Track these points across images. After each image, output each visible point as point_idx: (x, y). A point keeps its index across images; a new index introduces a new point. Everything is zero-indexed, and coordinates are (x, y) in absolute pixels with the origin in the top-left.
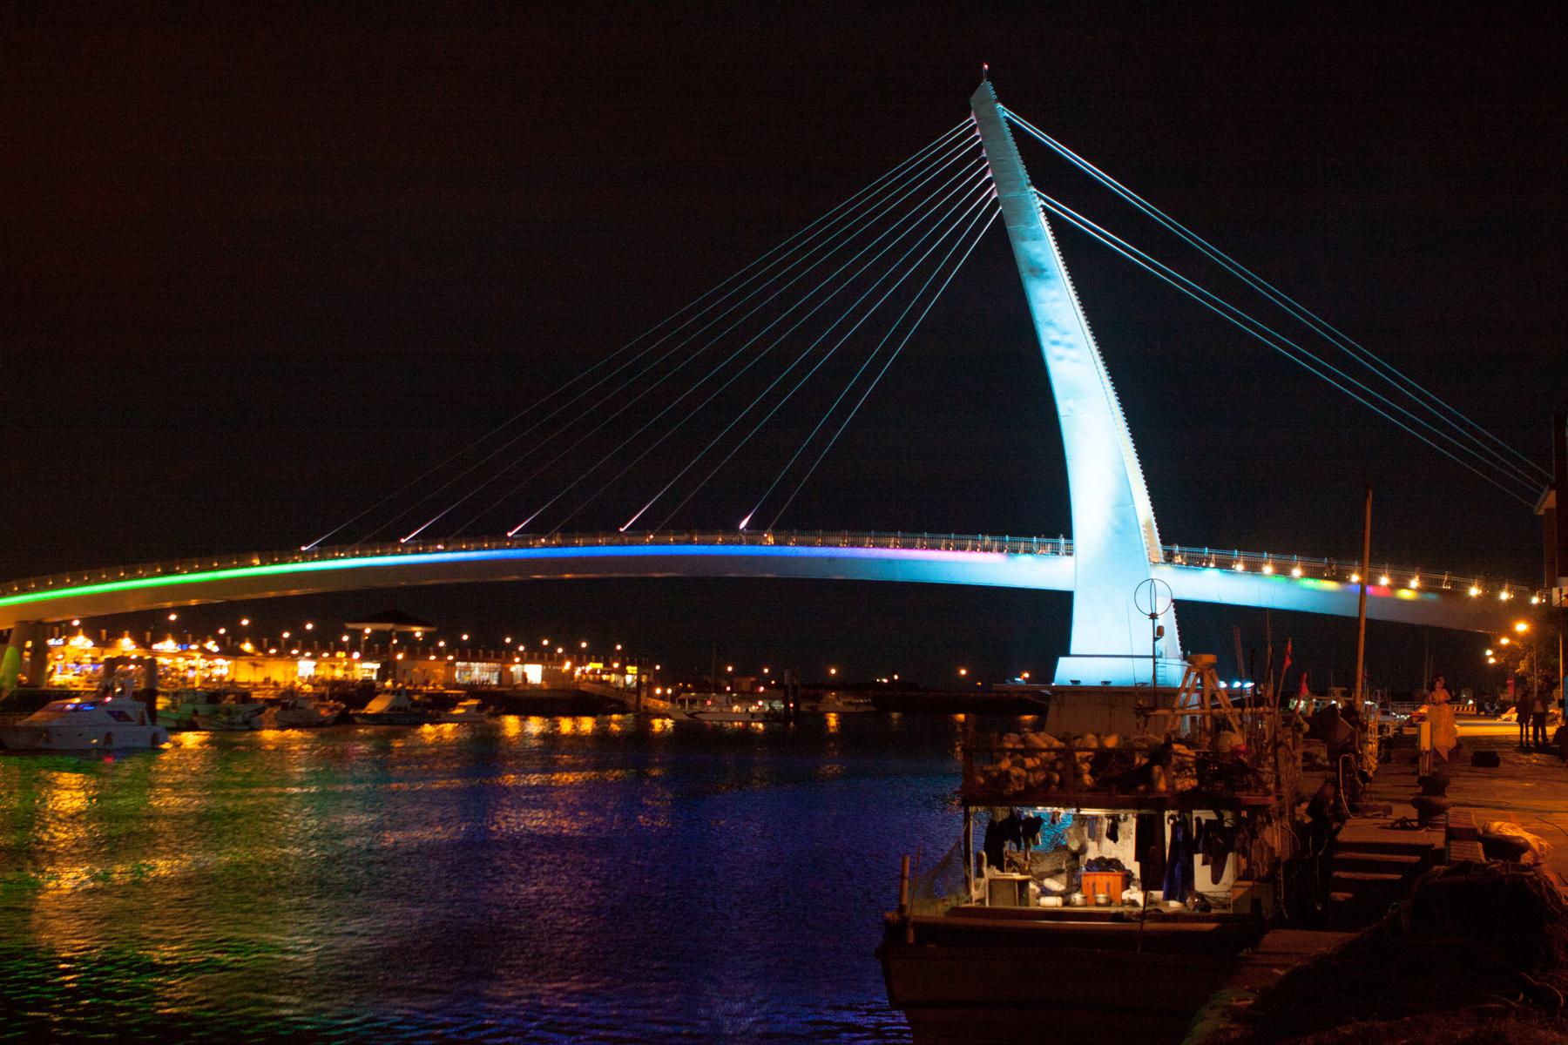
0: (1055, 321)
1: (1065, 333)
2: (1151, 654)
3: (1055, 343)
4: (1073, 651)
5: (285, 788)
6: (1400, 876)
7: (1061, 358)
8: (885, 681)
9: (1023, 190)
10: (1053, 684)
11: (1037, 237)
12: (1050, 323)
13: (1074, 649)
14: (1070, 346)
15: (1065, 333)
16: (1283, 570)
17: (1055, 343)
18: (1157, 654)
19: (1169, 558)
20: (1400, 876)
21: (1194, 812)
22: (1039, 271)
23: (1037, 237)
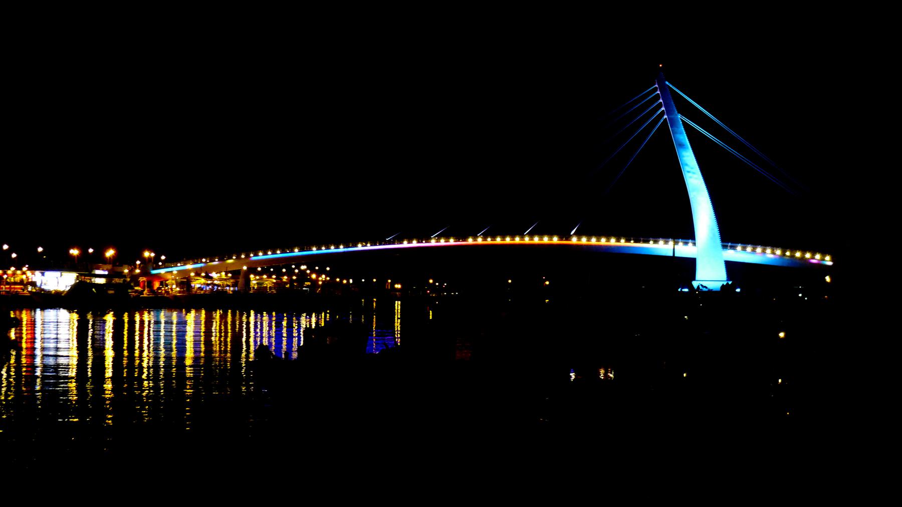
0: (688, 164)
1: (692, 168)
2: (59, 321)
3: (689, 172)
4: (696, 279)
5: (148, 288)
6: (431, 312)
7: (691, 177)
8: (686, 290)
9: (676, 115)
10: (91, 313)
11: (681, 133)
12: (687, 165)
13: (697, 279)
14: (694, 173)
15: (692, 168)
16: (744, 249)
17: (689, 172)
18: (56, 321)
19: (724, 247)
20: (431, 312)
21: (122, 282)
22: (682, 145)
23: (681, 133)
